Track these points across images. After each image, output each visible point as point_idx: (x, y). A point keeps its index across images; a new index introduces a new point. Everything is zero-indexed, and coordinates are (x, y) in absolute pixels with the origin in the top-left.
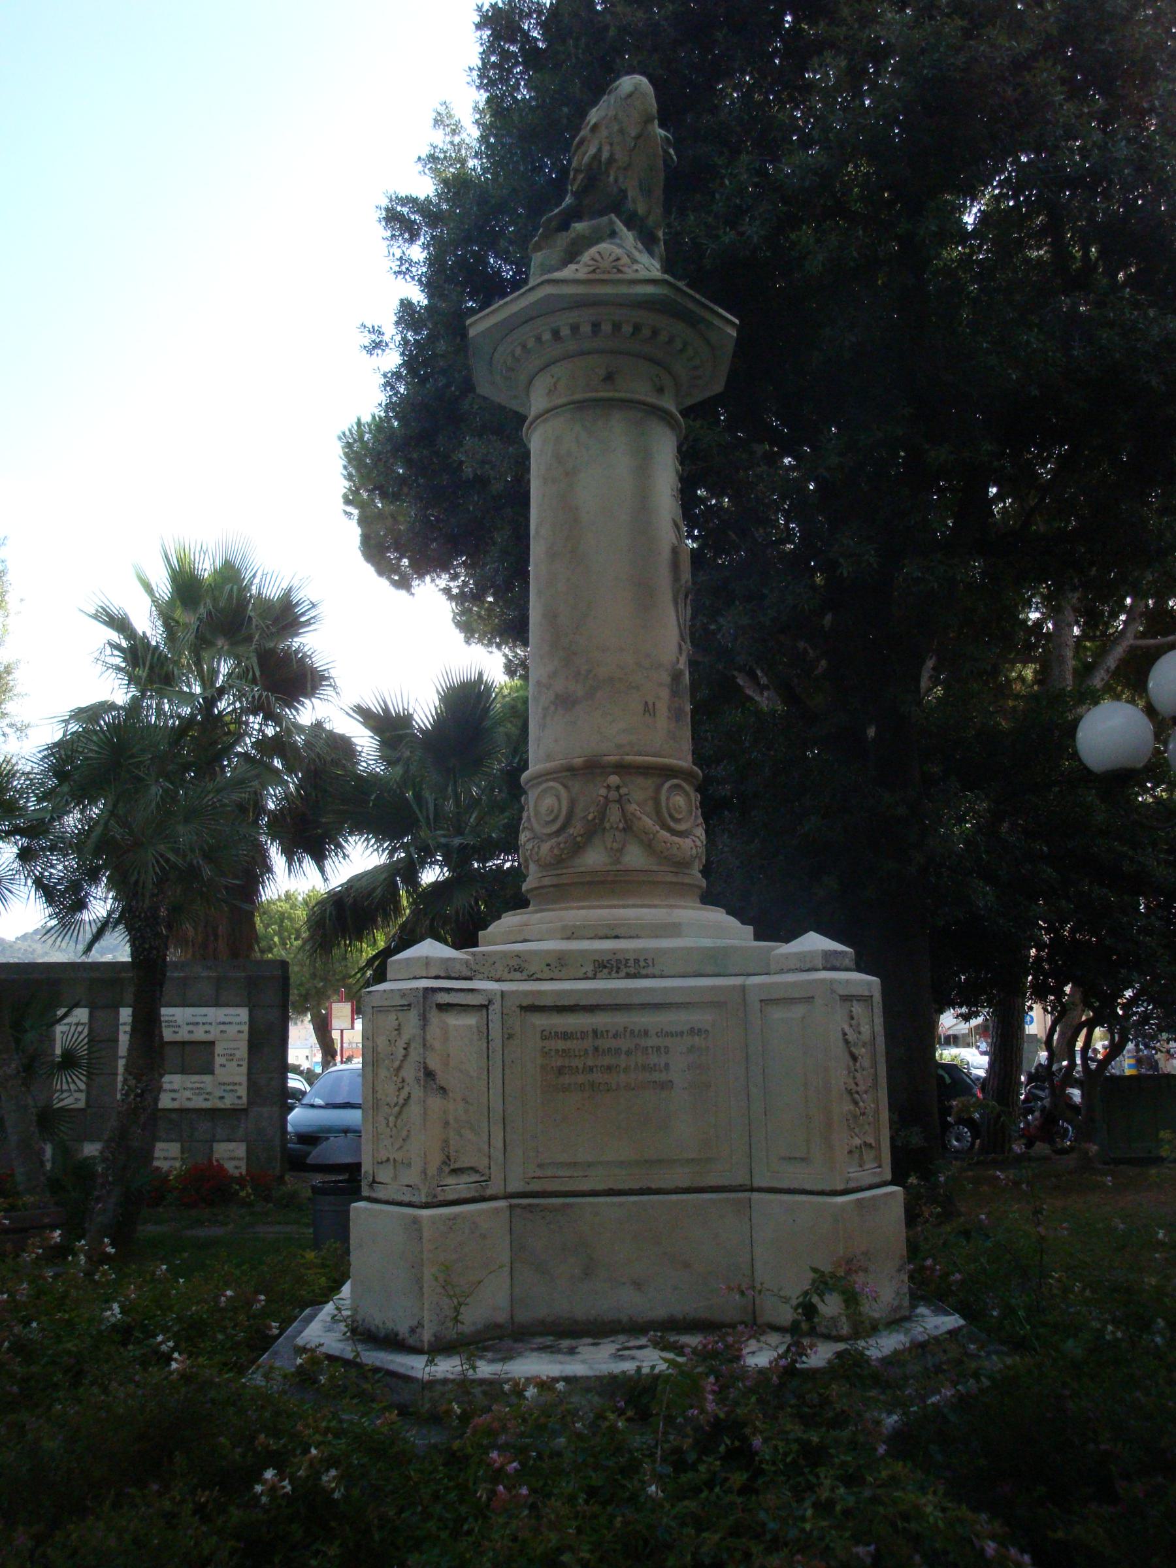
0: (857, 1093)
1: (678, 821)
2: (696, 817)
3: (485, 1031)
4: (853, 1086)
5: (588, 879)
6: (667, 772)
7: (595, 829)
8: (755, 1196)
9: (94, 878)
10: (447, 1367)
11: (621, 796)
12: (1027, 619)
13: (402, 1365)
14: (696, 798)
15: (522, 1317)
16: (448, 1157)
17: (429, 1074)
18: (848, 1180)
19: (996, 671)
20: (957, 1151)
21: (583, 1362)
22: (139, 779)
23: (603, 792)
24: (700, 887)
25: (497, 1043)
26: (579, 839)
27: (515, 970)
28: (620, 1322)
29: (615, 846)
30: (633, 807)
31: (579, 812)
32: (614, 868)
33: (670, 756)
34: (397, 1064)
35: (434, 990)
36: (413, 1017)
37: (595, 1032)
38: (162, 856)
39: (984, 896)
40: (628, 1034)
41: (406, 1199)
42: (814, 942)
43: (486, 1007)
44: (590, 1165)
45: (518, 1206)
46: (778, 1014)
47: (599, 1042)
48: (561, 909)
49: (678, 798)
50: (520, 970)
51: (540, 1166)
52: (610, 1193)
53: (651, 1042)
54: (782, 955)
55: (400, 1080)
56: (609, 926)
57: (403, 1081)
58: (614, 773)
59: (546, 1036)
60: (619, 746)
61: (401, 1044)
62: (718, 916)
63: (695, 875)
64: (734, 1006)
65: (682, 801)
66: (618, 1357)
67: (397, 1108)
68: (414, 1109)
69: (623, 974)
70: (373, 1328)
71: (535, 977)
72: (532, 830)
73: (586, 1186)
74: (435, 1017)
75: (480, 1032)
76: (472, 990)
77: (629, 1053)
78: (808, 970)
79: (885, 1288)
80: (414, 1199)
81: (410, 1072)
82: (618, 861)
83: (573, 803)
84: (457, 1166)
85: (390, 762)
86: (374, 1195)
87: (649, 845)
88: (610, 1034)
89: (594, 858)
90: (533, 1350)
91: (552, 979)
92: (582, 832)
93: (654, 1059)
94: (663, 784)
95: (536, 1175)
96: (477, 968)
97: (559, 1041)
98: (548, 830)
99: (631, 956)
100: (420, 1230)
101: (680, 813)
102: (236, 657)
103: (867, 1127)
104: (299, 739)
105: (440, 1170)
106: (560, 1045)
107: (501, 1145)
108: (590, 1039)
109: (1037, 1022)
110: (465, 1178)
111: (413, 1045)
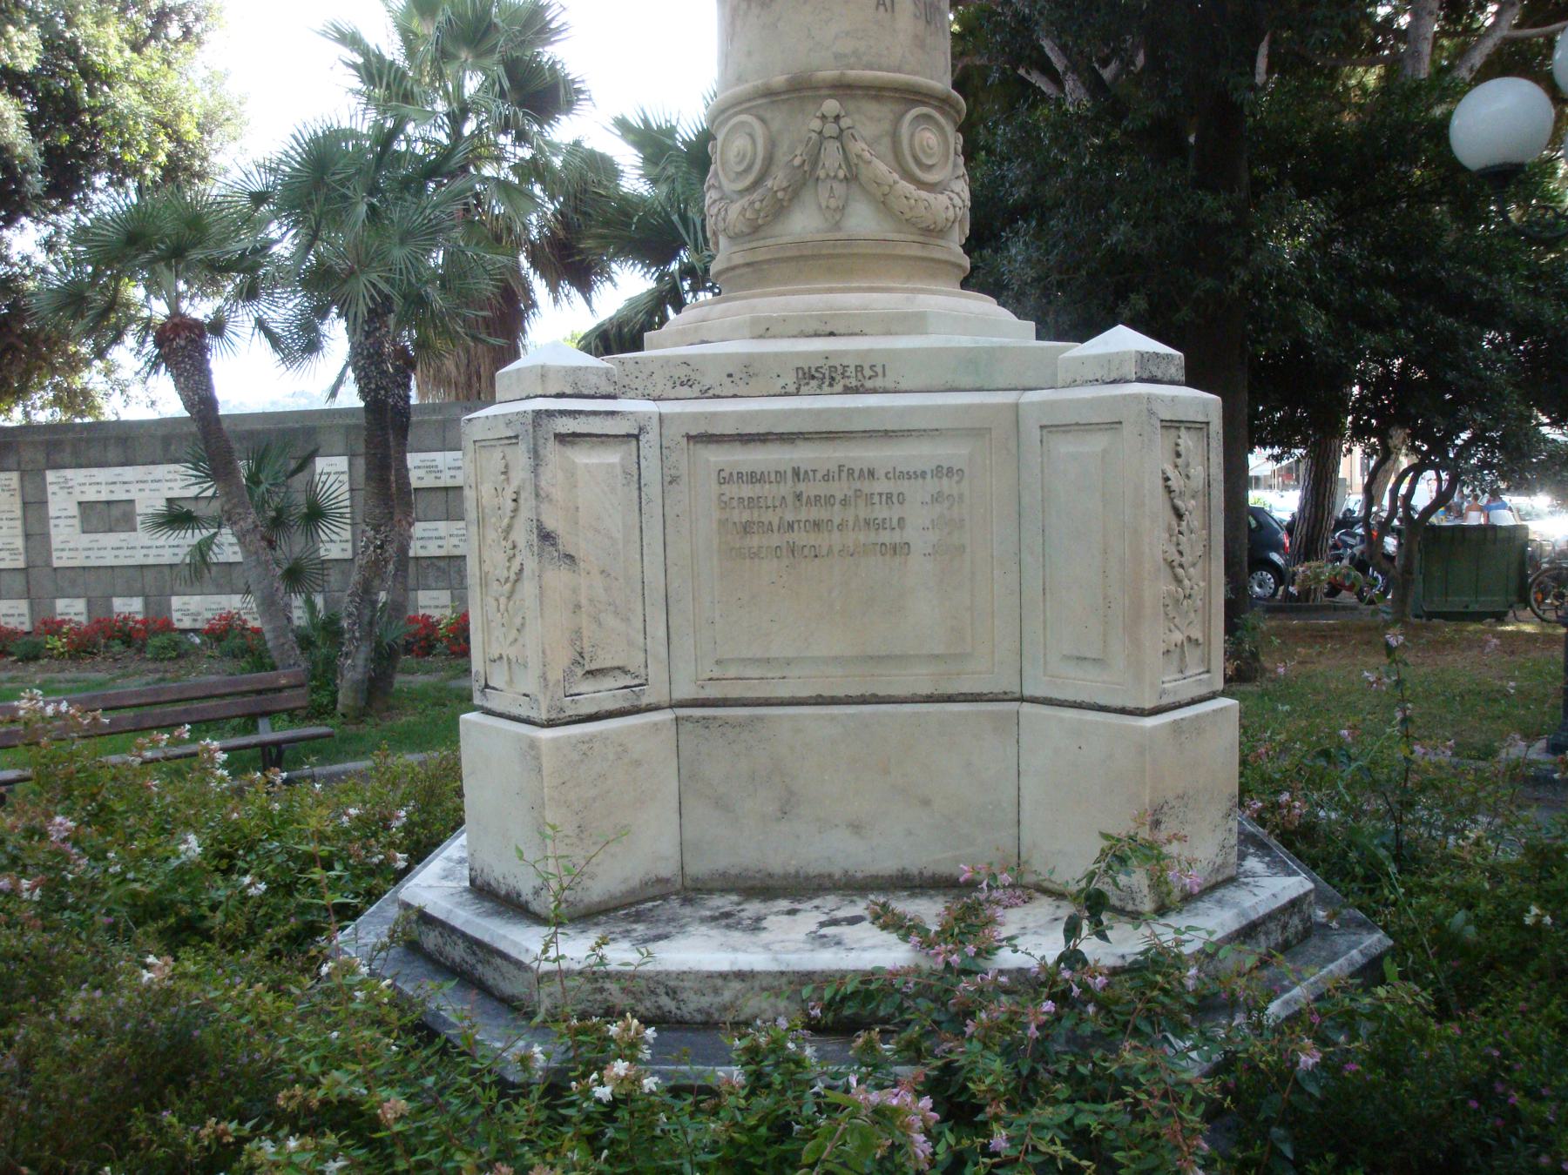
0: (1181, 566)
1: (930, 168)
2: (955, 165)
3: (635, 473)
4: (1177, 557)
5: (794, 253)
6: (911, 96)
7: (805, 178)
8: (1026, 708)
9: (322, 312)
10: (576, 949)
11: (841, 131)
12: (1374, 15)
13: (515, 944)
14: (956, 141)
15: (699, 867)
16: (581, 654)
17: (546, 537)
18: (1164, 692)
19: (1333, 75)
20: (1259, 598)
21: (767, 947)
22: (345, 197)
23: (816, 124)
24: (960, 266)
25: (653, 489)
26: (780, 195)
27: (682, 384)
28: (830, 876)
29: (833, 203)
30: (858, 147)
31: (782, 156)
32: (831, 236)
33: (916, 73)
34: (506, 521)
35: (550, 414)
36: (520, 457)
37: (796, 473)
38: (374, 285)
39: (1314, 324)
40: (844, 475)
41: (523, 712)
42: (1123, 340)
43: (637, 437)
44: (789, 662)
45: (688, 719)
46: (1065, 447)
47: (802, 487)
48: (754, 296)
49: (928, 134)
50: (687, 383)
51: (718, 662)
52: (819, 701)
53: (881, 486)
54: (1074, 359)
55: (509, 545)
56: (820, 318)
57: (514, 547)
58: (830, 97)
59: (724, 479)
60: (837, 56)
61: (509, 494)
62: (984, 306)
63: (954, 247)
64: (1002, 434)
65: (938, 142)
66: (819, 940)
67: (508, 585)
68: (528, 588)
69: (838, 387)
70: (493, 882)
71: (711, 393)
72: (720, 188)
73: (784, 692)
74: (552, 451)
75: (626, 473)
76: (613, 413)
77: (845, 502)
78: (1114, 382)
79: (1204, 842)
80: (533, 714)
81: (523, 534)
82: (837, 226)
83: (772, 145)
84: (594, 666)
85: (654, 181)
86: (488, 705)
87: (884, 203)
88: (819, 476)
89: (803, 223)
90: (703, 920)
91: (735, 396)
92: (785, 184)
93: (881, 512)
94: (902, 115)
95: (715, 675)
96: (626, 381)
97: (744, 486)
98: (740, 186)
99: (852, 363)
100: (537, 758)
101: (931, 156)
102: (484, 70)
103: (1192, 615)
104: (557, 162)
105: (568, 675)
106: (747, 491)
107: (662, 633)
108: (790, 482)
109: (1352, 466)
110: (609, 682)
111: (523, 495)
